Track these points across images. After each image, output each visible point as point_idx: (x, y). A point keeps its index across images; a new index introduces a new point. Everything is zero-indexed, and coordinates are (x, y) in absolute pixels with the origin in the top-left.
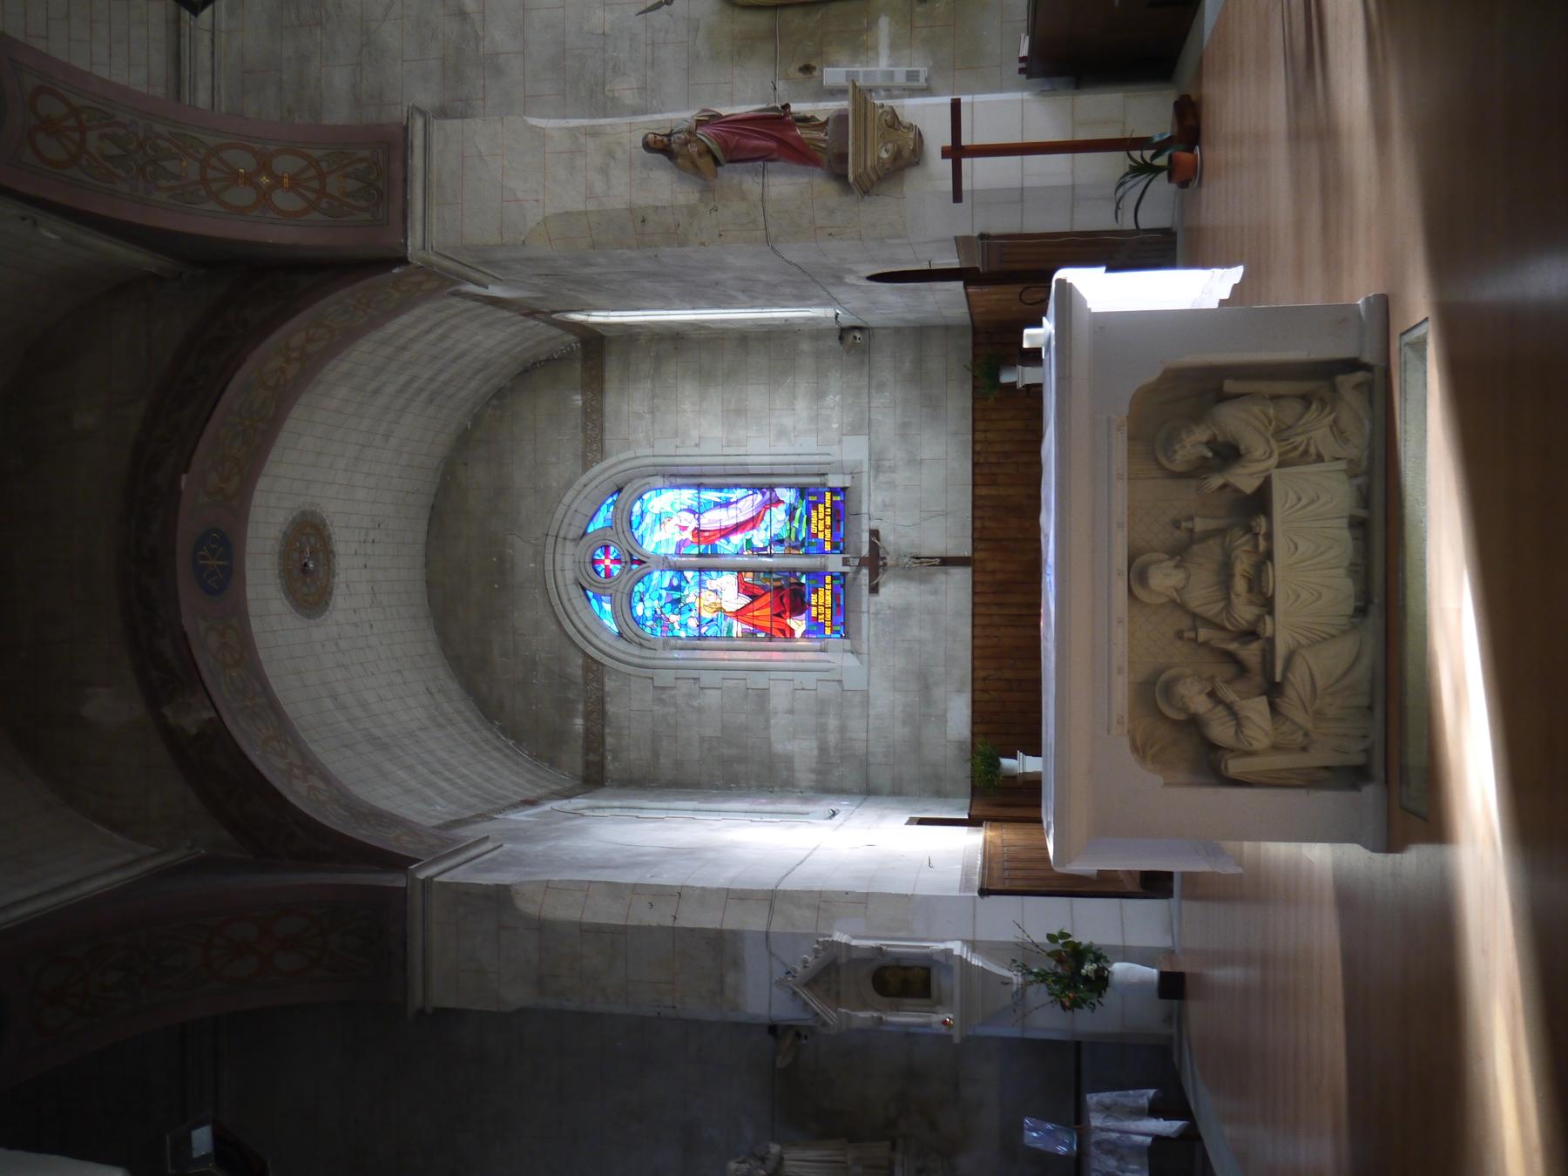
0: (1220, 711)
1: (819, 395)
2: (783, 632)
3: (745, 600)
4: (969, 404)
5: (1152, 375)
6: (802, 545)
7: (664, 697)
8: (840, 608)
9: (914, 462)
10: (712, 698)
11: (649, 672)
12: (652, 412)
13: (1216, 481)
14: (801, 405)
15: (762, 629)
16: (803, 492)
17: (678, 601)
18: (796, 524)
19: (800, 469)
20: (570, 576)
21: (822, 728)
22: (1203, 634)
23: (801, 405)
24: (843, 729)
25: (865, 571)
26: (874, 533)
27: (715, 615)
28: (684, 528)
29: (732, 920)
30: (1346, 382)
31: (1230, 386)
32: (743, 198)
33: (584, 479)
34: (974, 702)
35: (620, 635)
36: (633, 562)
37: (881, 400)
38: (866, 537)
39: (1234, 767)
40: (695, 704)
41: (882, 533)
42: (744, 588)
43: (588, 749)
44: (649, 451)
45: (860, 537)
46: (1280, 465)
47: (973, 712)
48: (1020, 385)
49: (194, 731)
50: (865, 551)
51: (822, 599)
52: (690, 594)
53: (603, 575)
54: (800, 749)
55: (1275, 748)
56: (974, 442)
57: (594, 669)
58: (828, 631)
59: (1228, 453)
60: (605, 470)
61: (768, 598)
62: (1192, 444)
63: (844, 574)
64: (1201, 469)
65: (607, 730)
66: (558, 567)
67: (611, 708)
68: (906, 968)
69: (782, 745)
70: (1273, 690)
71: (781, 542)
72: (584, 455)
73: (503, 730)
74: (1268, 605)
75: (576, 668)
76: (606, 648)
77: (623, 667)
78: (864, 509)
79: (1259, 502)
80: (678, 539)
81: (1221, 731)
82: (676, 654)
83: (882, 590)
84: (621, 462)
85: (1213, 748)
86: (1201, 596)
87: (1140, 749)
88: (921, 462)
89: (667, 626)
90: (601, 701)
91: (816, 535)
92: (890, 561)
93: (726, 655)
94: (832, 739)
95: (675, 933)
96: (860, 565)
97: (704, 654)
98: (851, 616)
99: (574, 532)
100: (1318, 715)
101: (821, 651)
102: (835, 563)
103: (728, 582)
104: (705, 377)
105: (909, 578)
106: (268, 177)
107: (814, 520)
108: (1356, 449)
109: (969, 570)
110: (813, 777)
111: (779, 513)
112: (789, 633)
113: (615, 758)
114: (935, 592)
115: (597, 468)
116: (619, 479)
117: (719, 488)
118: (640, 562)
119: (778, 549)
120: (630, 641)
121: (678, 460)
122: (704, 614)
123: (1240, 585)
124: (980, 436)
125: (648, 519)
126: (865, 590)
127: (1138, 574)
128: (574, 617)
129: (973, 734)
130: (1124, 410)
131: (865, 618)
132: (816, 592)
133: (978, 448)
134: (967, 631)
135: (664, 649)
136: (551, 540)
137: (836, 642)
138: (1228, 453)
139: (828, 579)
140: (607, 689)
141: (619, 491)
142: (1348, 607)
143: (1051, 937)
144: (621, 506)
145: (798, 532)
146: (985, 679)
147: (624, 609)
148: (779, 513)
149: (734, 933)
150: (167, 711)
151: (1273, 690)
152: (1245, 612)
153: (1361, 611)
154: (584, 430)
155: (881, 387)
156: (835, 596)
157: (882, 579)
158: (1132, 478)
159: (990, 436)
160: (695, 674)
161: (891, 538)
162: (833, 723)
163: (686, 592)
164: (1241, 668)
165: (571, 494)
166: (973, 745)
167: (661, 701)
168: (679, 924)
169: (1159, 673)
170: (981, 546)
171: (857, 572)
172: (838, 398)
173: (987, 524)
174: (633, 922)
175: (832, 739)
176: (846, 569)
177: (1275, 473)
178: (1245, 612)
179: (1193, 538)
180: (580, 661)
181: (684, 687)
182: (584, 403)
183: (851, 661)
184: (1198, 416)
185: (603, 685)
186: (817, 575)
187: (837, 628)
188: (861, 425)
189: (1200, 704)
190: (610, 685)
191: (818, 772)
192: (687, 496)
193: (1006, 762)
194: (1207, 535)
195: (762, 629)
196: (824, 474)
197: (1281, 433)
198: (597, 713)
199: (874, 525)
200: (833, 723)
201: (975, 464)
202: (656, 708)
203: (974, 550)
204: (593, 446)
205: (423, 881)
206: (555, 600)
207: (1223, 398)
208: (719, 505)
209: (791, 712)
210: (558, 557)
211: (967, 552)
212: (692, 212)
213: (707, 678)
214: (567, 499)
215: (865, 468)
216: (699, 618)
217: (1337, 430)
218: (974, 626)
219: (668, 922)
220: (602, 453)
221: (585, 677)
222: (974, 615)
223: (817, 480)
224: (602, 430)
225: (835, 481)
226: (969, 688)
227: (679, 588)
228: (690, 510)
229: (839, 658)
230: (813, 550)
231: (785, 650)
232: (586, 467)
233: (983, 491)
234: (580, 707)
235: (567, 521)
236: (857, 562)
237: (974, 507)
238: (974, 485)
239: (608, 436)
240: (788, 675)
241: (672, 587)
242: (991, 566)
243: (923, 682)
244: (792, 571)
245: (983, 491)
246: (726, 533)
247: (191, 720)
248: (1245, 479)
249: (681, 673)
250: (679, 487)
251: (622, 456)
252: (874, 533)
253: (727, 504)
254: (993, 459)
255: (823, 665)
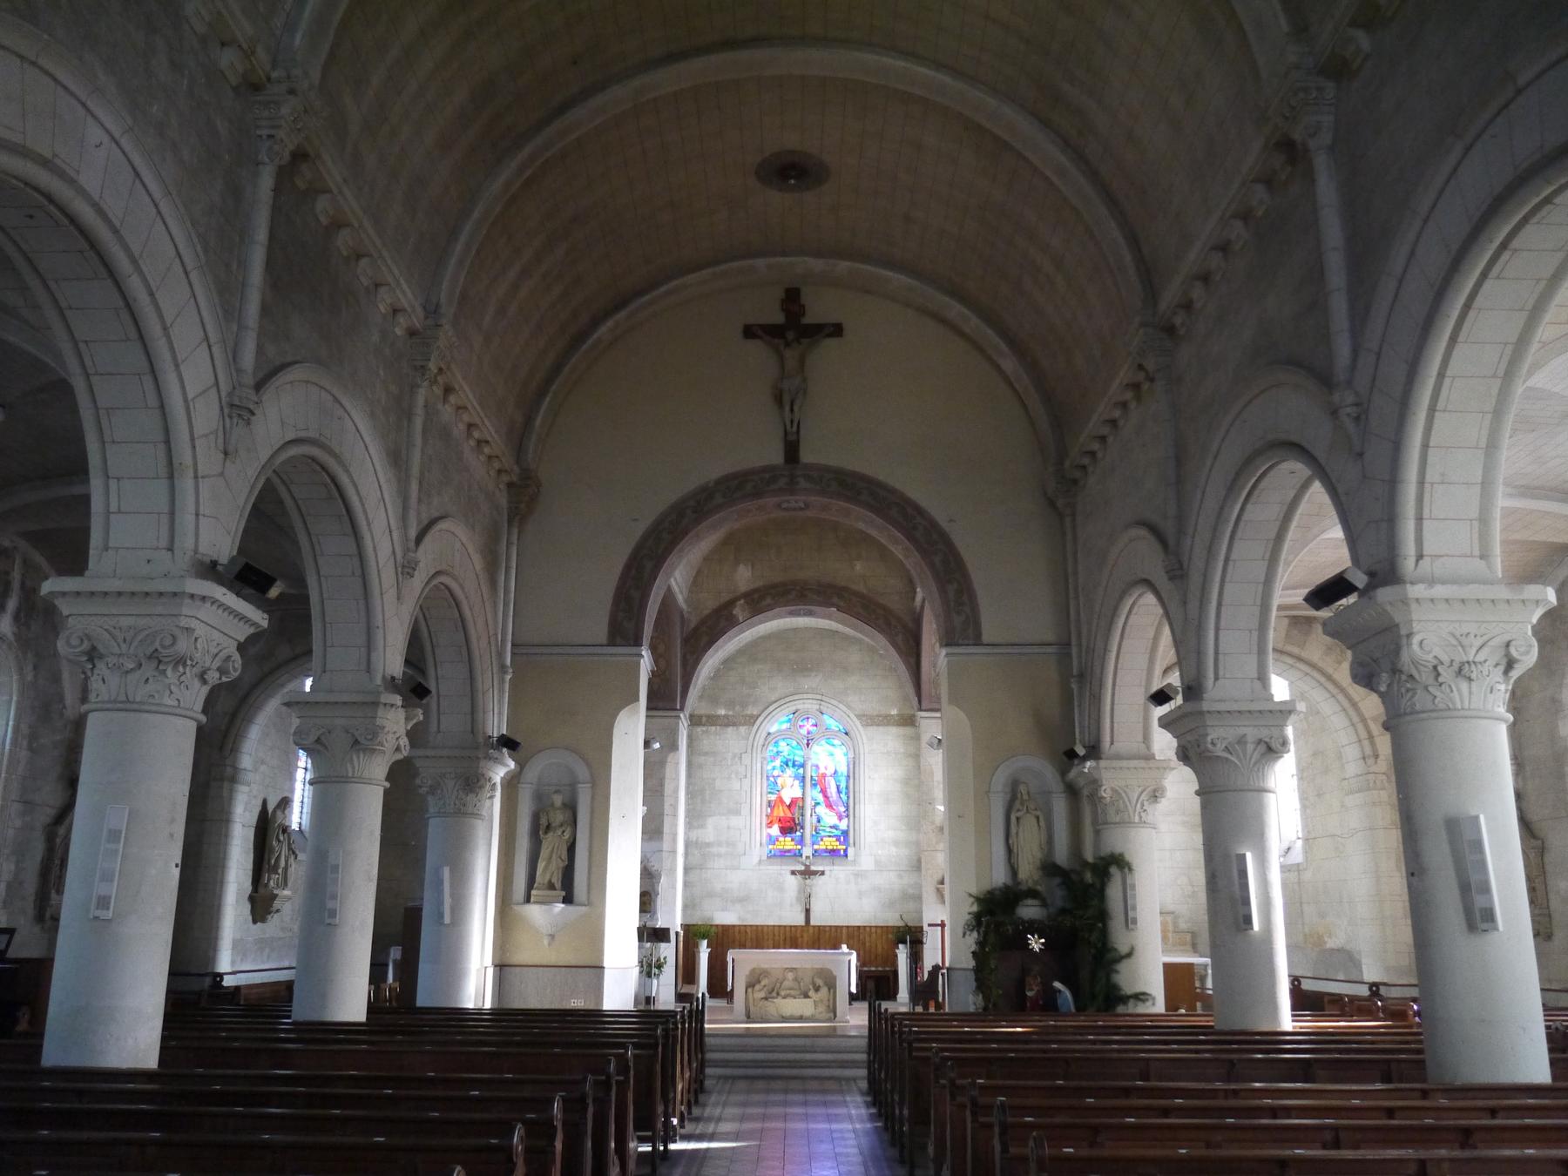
0: (761, 987)
1: (896, 843)
2: (771, 822)
3: (788, 803)
4: (891, 924)
5: (835, 973)
6: (817, 833)
7: (737, 759)
8: (783, 854)
9: (860, 894)
10: (736, 785)
11: (749, 750)
12: (888, 752)
13: (811, 987)
14: (890, 834)
15: (772, 811)
16: (845, 833)
17: (787, 765)
18: (828, 830)
19: (857, 832)
20: (799, 707)
21: (720, 844)
22: (778, 985)
23: (890, 834)
24: (719, 855)
25: (803, 868)
26: (823, 873)
27: (779, 785)
28: (826, 768)
29: (666, 837)
30: (832, 1015)
31: (832, 991)
32: (937, 843)
33: (852, 716)
34: (734, 926)
35: (769, 734)
36: (808, 740)
37: (893, 876)
38: (820, 868)
39: (750, 990)
40: (733, 776)
41: (822, 877)
42: (794, 801)
43: (709, 717)
44: (867, 751)
45: (821, 865)
46: (814, 1001)
47: (729, 926)
48: (897, 951)
49: (734, 612)
50: (813, 868)
51: (788, 843)
52: (790, 771)
53: (801, 724)
54: (709, 833)
55: (754, 1000)
56: (870, 927)
57: (751, 720)
58: (771, 847)
59: (817, 989)
60: (857, 728)
61: (789, 815)
62: (819, 982)
63: (801, 856)
64: (814, 984)
65: (718, 727)
66: (805, 701)
67: (730, 729)
68: (650, 904)
69: (711, 822)
70: (766, 999)
71: (819, 821)
72: (864, 715)
73: (718, 670)
74: (784, 998)
75: (755, 711)
76: (761, 728)
77: (751, 739)
78: (835, 867)
79: (806, 996)
80: (820, 766)
81: (757, 987)
82: (759, 765)
83: (793, 876)
84: (861, 735)
85: (753, 986)
86: (786, 984)
87: (753, 970)
88: (860, 898)
89: (774, 758)
90: (734, 724)
91: (822, 840)
92: (808, 881)
93: (759, 789)
94: (714, 850)
95: (662, 814)
96: (806, 865)
97: (759, 780)
98: (779, 860)
99: (824, 709)
100: (761, 1008)
101: (761, 844)
102: (807, 851)
103: (798, 793)
104: (906, 782)
105: (799, 892)
106: (679, 1121)
107: (831, 839)
108: (818, 1016)
109: (803, 924)
110: (694, 839)
111: (834, 820)
112: (770, 825)
113: (703, 731)
114: (791, 905)
115: (858, 722)
116: (852, 733)
117: (847, 788)
118: (808, 745)
119: (815, 819)
120: (766, 739)
121: (862, 766)
122: (779, 778)
123: (788, 992)
124: (873, 930)
125: (831, 748)
126: (793, 868)
127: (792, 970)
128: (778, 709)
129: (717, 926)
130: (828, 967)
131: (779, 867)
132: (792, 840)
133: (868, 929)
134: (771, 923)
135: (762, 758)
136: (819, 697)
137: (766, 851)
138: (817, 989)
139: (799, 847)
140: (741, 727)
141: (846, 734)
142: (784, 1015)
143: (665, 958)
144: (838, 734)
145: (824, 830)
146: (746, 932)
147: (783, 735)
148: (834, 820)
149: (662, 838)
150: (742, 601)
151: (766, 999)
152: (783, 993)
153: (783, 1017)
154: (879, 716)
155: (900, 877)
156: (789, 851)
157: (799, 877)
158: (813, 969)
159: (874, 935)
160: (749, 776)
161: (820, 882)
162: (723, 850)
163: (791, 769)
164: (770, 993)
165: (845, 709)
166: (711, 926)
167: (734, 756)
168: (665, 817)
169: (767, 972)
170: (816, 930)
171: (803, 864)
172: (894, 854)
173: (827, 934)
174: (665, 798)
175: (714, 850)
176: (804, 857)
177: (812, 1000)
178: (783, 993)
179: (799, 983)
180: (755, 713)
181: (742, 770)
182: (892, 715)
183: (756, 860)
184: (826, 984)
185: (743, 725)
186: (801, 842)
187: (773, 852)
188: (880, 866)
189: (763, 983)
190: (743, 729)
191: (697, 843)
192: (843, 770)
193: (705, 942)
194: (800, 985)
195: (772, 811)
196: (854, 844)
197: (822, 1001)
198: (728, 722)
199: (827, 873)
200: (723, 850)
201: (859, 927)
202: (730, 754)
203: (814, 927)
204: (870, 720)
205: (679, 716)
206: (787, 700)
207: (829, 989)
208: (838, 787)
209: (729, 828)
210: (810, 701)
211: (813, 923)
212: (933, 823)
213: (746, 782)
214: (841, 706)
215: (857, 868)
216: (778, 776)
217: (821, 1013)
218: (774, 926)
219: (666, 812)
220: (866, 725)
221: (747, 715)
222: (780, 926)
223: (851, 841)
224: (878, 725)
225: (851, 851)
226: (740, 923)
227: (794, 765)
228: (836, 772)
229: (758, 852)
230: (815, 839)
231: (761, 824)
232: (859, 717)
233: (844, 931)
234: (731, 713)
235: (830, 706)
236: (808, 864)
237: (836, 927)
238: (848, 927)
239: (875, 728)
240: (748, 827)
241: (794, 762)
242: (805, 935)
243: (743, 900)
244: (802, 828)
245: (844, 931)
246: (824, 792)
247: (737, 611)
248: (811, 993)
249: (749, 768)
250: (848, 766)
251: (864, 738)
252: (823, 873)
253: (839, 792)
254: (861, 937)
255: (753, 846)
